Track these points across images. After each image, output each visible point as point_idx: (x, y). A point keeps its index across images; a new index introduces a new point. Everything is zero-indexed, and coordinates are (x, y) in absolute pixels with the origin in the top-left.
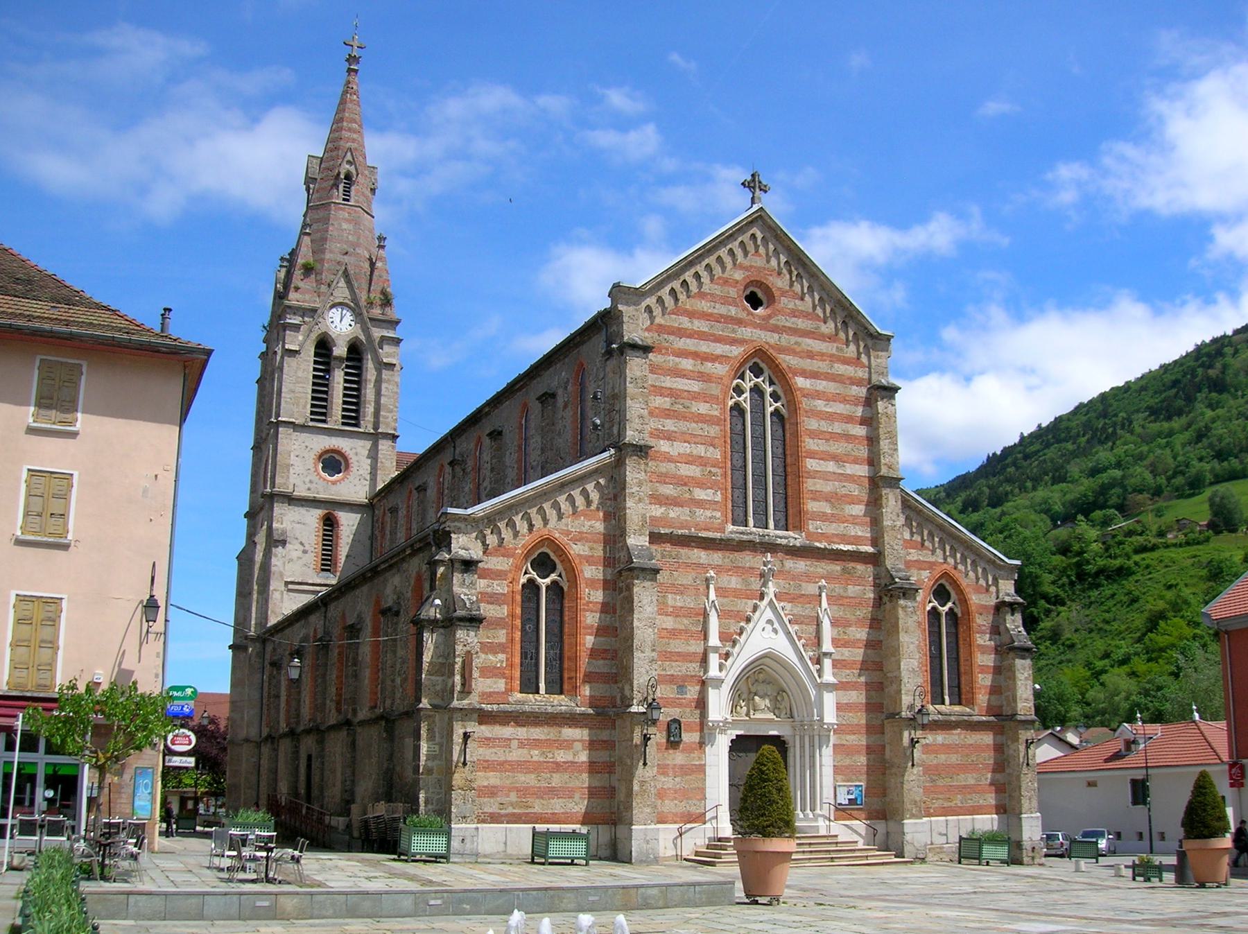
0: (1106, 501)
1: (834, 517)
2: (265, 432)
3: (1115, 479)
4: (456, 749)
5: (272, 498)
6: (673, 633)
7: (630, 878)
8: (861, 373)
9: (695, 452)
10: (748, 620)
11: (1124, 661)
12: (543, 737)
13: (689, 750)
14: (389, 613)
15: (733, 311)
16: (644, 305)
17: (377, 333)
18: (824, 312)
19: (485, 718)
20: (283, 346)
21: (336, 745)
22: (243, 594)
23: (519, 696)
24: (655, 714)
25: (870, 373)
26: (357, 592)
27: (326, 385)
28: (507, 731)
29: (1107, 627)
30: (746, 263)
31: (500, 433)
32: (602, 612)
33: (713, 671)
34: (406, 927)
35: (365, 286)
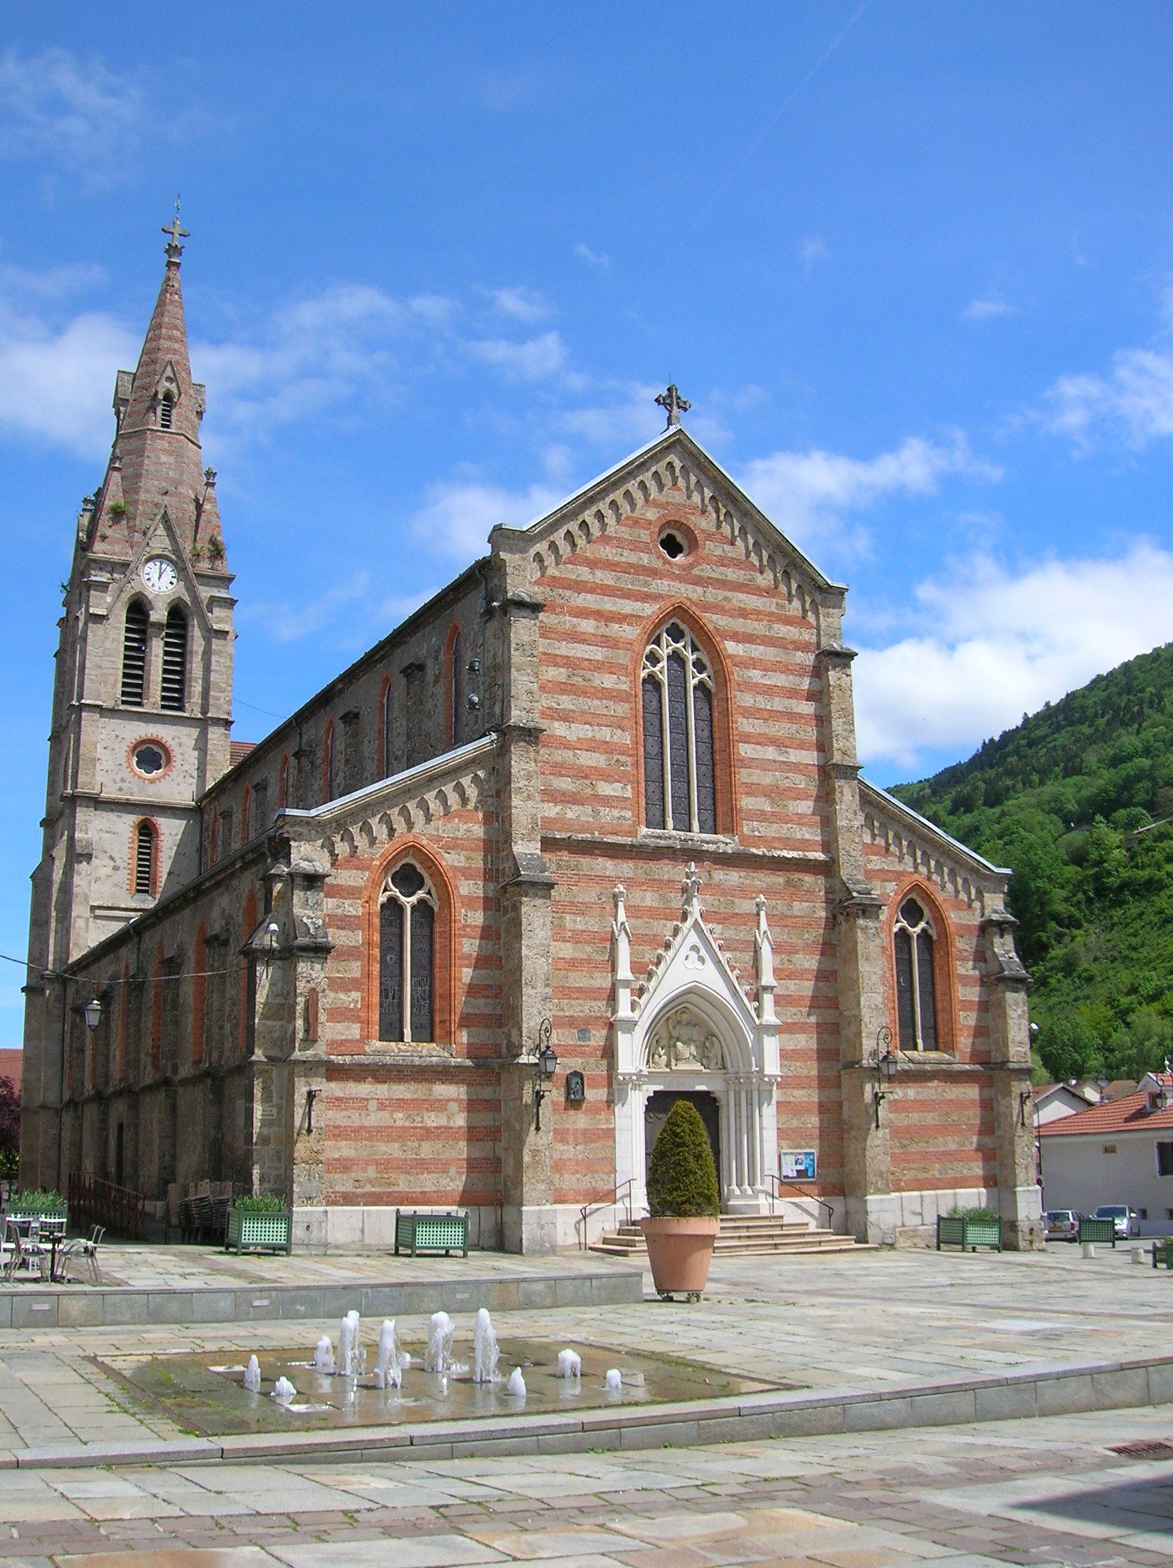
0: (1132, 796)
1: (775, 815)
2: (65, 718)
3: (1142, 770)
4: (299, 1112)
5: (73, 801)
6: (573, 964)
7: (516, 1272)
8: (808, 636)
9: (598, 737)
10: (667, 946)
11: (1155, 997)
12: (408, 1096)
13: (594, 1110)
14: (214, 942)
15: (645, 559)
16: (532, 552)
17: (205, 592)
18: (761, 560)
19: (334, 1072)
20: (87, 610)
21: (153, 1111)
22: (39, 923)
23: (379, 1045)
24: (550, 1066)
25: (819, 635)
26: (178, 917)
27: (142, 659)
28: (364, 1089)
29: (1134, 955)
30: (662, 499)
31: (357, 715)
32: (482, 938)
33: (624, 1011)
34: (221, 1333)
35: (189, 533)
